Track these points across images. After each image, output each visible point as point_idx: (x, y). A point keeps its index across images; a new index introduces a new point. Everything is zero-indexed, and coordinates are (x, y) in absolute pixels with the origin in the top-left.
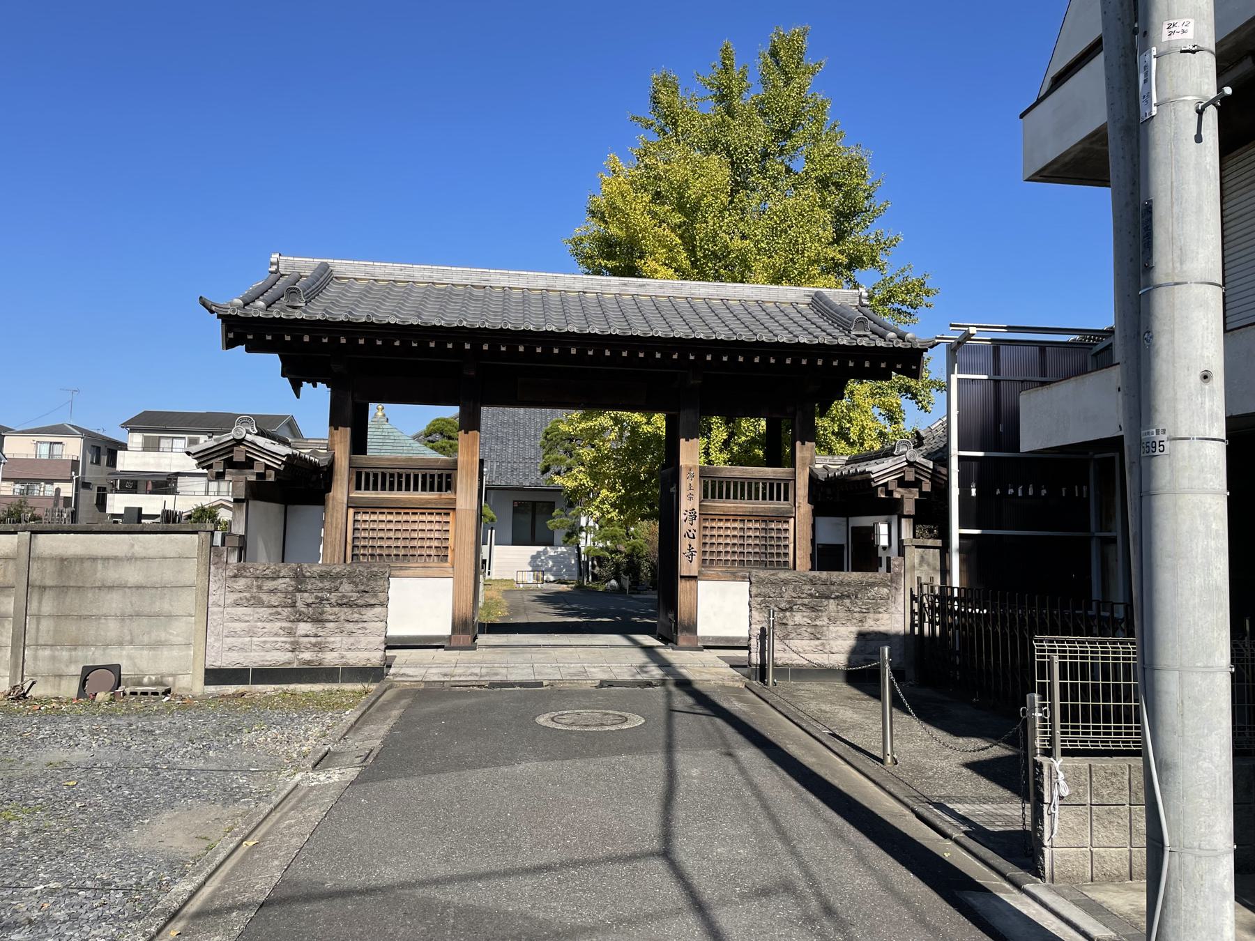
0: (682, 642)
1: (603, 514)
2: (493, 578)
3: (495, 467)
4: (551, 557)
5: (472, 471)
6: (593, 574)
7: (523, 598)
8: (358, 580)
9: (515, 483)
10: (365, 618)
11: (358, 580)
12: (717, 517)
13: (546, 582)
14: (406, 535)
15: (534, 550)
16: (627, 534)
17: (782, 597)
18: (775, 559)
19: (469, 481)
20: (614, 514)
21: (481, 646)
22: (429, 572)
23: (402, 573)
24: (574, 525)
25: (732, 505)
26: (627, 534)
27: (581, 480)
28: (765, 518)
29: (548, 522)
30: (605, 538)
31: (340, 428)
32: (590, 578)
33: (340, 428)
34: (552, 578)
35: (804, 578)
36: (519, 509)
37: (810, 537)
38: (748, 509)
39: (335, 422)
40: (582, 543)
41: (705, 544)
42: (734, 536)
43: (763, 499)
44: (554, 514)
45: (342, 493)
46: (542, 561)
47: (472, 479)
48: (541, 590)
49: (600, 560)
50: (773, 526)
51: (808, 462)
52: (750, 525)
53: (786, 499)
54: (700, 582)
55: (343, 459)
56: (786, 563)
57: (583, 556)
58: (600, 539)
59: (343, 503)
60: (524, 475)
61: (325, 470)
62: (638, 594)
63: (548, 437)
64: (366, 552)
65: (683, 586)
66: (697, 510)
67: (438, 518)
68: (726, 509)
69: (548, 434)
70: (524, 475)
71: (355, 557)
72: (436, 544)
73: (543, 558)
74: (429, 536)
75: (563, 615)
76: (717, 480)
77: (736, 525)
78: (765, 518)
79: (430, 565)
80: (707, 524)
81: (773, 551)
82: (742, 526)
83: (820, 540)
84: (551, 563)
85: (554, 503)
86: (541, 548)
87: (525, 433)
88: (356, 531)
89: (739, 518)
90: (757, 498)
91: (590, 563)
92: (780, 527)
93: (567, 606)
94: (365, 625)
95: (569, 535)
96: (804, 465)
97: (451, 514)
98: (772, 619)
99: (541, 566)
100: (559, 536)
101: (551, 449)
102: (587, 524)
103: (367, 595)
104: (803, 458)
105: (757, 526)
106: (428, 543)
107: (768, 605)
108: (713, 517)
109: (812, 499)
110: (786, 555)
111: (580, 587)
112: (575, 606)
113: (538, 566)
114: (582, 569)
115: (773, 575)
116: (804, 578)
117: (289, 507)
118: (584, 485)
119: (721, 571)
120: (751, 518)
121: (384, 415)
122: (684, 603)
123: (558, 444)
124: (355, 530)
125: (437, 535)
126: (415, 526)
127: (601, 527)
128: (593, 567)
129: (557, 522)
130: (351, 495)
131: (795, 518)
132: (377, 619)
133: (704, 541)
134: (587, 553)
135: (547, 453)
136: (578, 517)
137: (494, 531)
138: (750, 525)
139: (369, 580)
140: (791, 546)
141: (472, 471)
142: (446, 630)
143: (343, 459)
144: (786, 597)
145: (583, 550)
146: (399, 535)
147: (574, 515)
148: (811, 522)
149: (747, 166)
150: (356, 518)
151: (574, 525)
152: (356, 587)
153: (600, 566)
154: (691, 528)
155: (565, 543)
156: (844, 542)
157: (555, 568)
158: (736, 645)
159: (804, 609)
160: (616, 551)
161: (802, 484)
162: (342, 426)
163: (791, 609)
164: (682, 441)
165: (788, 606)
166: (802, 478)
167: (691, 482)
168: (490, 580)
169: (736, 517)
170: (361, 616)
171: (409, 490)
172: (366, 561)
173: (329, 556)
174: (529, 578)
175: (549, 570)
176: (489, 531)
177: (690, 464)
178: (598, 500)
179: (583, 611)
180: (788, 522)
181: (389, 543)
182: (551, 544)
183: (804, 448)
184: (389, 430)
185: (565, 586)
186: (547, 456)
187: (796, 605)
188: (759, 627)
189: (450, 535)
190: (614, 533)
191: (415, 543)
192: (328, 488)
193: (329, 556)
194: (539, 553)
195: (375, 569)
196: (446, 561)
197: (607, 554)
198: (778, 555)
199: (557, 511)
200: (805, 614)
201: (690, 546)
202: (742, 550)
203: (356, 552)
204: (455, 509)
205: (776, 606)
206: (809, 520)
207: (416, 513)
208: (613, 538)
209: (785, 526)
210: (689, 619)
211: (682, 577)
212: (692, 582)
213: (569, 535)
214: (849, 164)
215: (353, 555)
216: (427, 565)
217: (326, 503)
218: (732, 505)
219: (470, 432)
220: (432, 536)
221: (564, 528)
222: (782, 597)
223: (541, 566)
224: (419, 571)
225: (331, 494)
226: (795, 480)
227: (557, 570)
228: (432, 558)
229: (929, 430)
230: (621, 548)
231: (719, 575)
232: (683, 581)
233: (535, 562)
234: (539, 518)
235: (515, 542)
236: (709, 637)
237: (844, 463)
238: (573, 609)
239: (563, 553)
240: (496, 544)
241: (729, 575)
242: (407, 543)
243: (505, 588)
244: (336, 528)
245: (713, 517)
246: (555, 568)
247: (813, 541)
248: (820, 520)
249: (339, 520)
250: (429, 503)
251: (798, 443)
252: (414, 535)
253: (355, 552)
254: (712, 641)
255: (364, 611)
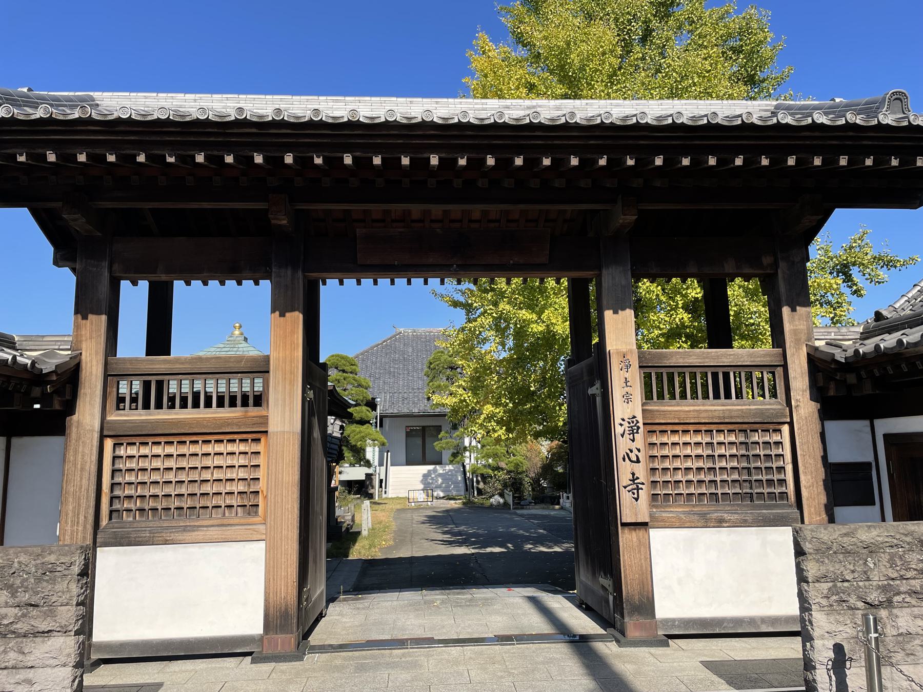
0: (632, 632)
1: (488, 432)
2: (390, 496)
3: (388, 397)
4: (440, 475)
5: (292, 373)
6: (478, 488)
7: (413, 519)
8: (18, 582)
9: (405, 411)
10: (30, 660)
11: (18, 582)
12: (669, 428)
13: (437, 498)
14: (194, 476)
15: (425, 469)
16: (507, 452)
17: (868, 579)
18: (766, 490)
19: (287, 387)
20: (501, 432)
21: (323, 649)
22: (230, 532)
23: (188, 536)
24: (458, 445)
25: (692, 408)
26: (507, 452)
27: (461, 395)
28: (744, 427)
29: (435, 444)
30: (488, 456)
31: (90, 316)
32: (476, 493)
33: (90, 316)
34: (442, 494)
35: (908, 539)
36: (410, 434)
37: (819, 453)
38: (716, 414)
39: (83, 307)
40: (467, 461)
41: (653, 470)
42: (699, 457)
43: (737, 398)
44: (440, 436)
45: (92, 415)
46: (432, 479)
47: (292, 383)
48: (430, 508)
49: (484, 478)
50: (755, 438)
51: (803, 337)
52: (721, 438)
53: (774, 395)
54: (653, 532)
55: (94, 363)
56: (783, 495)
57: (468, 474)
58: (483, 457)
59: (93, 431)
60: (414, 403)
61: (54, 378)
62: (523, 509)
63: (431, 366)
64: (132, 506)
65: (626, 538)
66: (640, 418)
67: (243, 447)
68: (682, 415)
69: (431, 364)
70: (414, 403)
71: (115, 515)
72: (241, 487)
73: (433, 476)
74: (229, 476)
75: (450, 543)
76: (664, 370)
77: (698, 439)
78: (744, 427)
79: (231, 522)
80: (654, 440)
81: (760, 477)
82: (708, 440)
83: (835, 457)
84: (440, 481)
85: (441, 426)
86: (431, 467)
87: (414, 367)
88: (117, 474)
89: (704, 428)
90: (728, 396)
91: (475, 479)
92: (767, 439)
93: (456, 530)
94: (30, 674)
95: (455, 455)
96: (797, 342)
97: (262, 440)
98: (873, 635)
99: (432, 483)
100: (446, 456)
101: (434, 377)
102: (470, 444)
103: (34, 612)
104: (795, 332)
105: (732, 438)
106: (229, 487)
107: (844, 597)
108: (663, 428)
109: (817, 392)
110: (782, 482)
111: (468, 503)
112: (462, 528)
113: (429, 483)
114: (468, 486)
115: (846, 535)
116: (908, 539)
117: (15, 441)
118: (465, 400)
119: (684, 513)
120: (722, 427)
121: (242, 334)
122: (631, 566)
123: (440, 372)
124: (114, 472)
125: (242, 474)
126: (208, 462)
127: (483, 446)
128: (478, 482)
129: (443, 443)
130: (109, 418)
131: (791, 424)
132: (52, 662)
133: (651, 466)
134: (474, 472)
135: (432, 381)
136: (462, 438)
137: (389, 453)
138: (721, 438)
139: (39, 580)
140: (789, 468)
141: (292, 373)
142: (256, 627)
143: (94, 363)
144: (877, 578)
145: (468, 468)
146: (182, 477)
147: (458, 436)
148: (818, 428)
149: (630, 37)
150: (117, 453)
151: (458, 445)
152: (13, 595)
153: (485, 483)
154: (633, 446)
155: (451, 462)
156: (870, 458)
157: (444, 485)
158: (717, 631)
159: (914, 602)
160: (498, 468)
161: (799, 370)
162: (93, 313)
163: (889, 603)
164: (608, 314)
165: (882, 598)
166: (797, 362)
167: (627, 375)
168: (386, 498)
169: (698, 427)
170: (21, 657)
171: (199, 407)
172: (131, 519)
173: (70, 514)
174: (421, 496)
175: (439, 487)
176: (386, 454)
177: (623, 348)
178: (482, 417)
179: (473, 535)
180: (780, 431)
181: (168, 490)
182: (439, 462)
183: (796, 315)
184: (245, 349)
185: (453, 502)
186: (431, 384)
187: (899, 593)
188: (830, 644)
189: (261, 474)
190: (495, 451)
191: (206, 488)
192: (70, 408)
193: (70, 514)
194: (429, 471)
195: (52, 558)
196: (256, 513)
197: (490, 472)
198: (770, 482)
199: (442, 434)
200: (916, 611)
201: (633, 474)
202: (712, 478)
203: (117, 506)
204: (266, 432)
205: (860, 598)
206: (816, 426)
207: (210, 441)
208: (495, 456)
209: (776, 438)
210: (640, 593)
211: (624, 525)
212: (641, 533)
213: (455, 455)
214: (747, 24)
215: (111, 512)
216: (225, 522)
217: (67, 432)
218: (692, 408)
219: (288, 314)
220: (234, 476)
221: (449, 449)
222: (868, 579)
223: (432, 483)
224: (214, 532)
225: (75, 417)
226: (785, 367)
227: (446, 487)
228: (234, 510)
229: (892, 309)
230: (502, 465)
231: (680, 519)
232: (626, 530)
233: (426, 480)
234: (428, 440)
235: (409, 462)
236: (674, 620)
237: (858, 336)
238: (460, 533)
239: (450, 471)
240: (391, 465)
241: (696, 517)
242: (195, 489)
243: (398, 507)
244: (82, 469)
245: (663, 428)
246: (444, 485)
247: (825, 458)
248: (830, 425)
249: (87, 458)
250: (229, 425)
251: (786, 310)
252: (206, 475)
253: (114, 507)
254: (679, 627)
255: (28, 644)
